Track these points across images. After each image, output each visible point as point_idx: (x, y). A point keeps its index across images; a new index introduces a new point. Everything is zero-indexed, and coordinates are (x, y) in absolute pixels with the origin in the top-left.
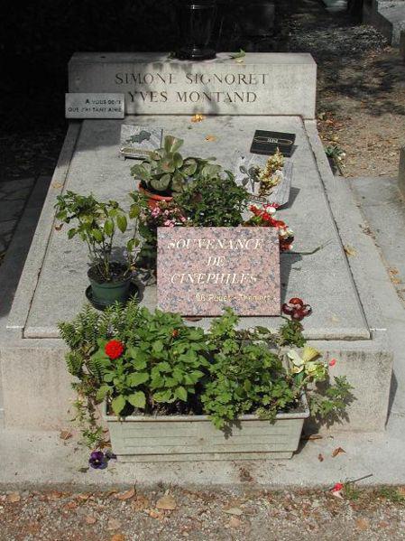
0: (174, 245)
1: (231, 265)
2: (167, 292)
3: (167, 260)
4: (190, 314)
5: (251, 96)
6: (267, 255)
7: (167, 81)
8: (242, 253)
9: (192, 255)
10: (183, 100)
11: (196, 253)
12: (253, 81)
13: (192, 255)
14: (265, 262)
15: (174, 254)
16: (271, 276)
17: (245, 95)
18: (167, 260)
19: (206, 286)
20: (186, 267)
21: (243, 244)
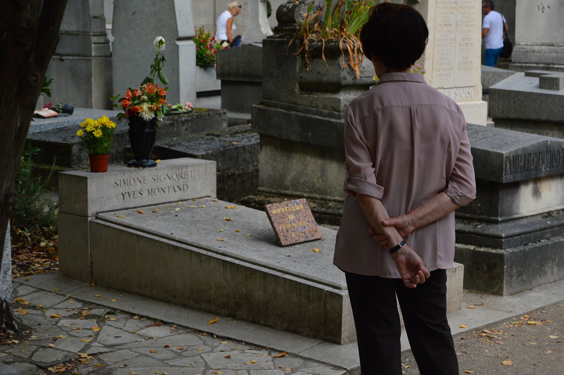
1: (298, 218)
10: (151, 193)
17: (182, 186)
18: (275, 220)
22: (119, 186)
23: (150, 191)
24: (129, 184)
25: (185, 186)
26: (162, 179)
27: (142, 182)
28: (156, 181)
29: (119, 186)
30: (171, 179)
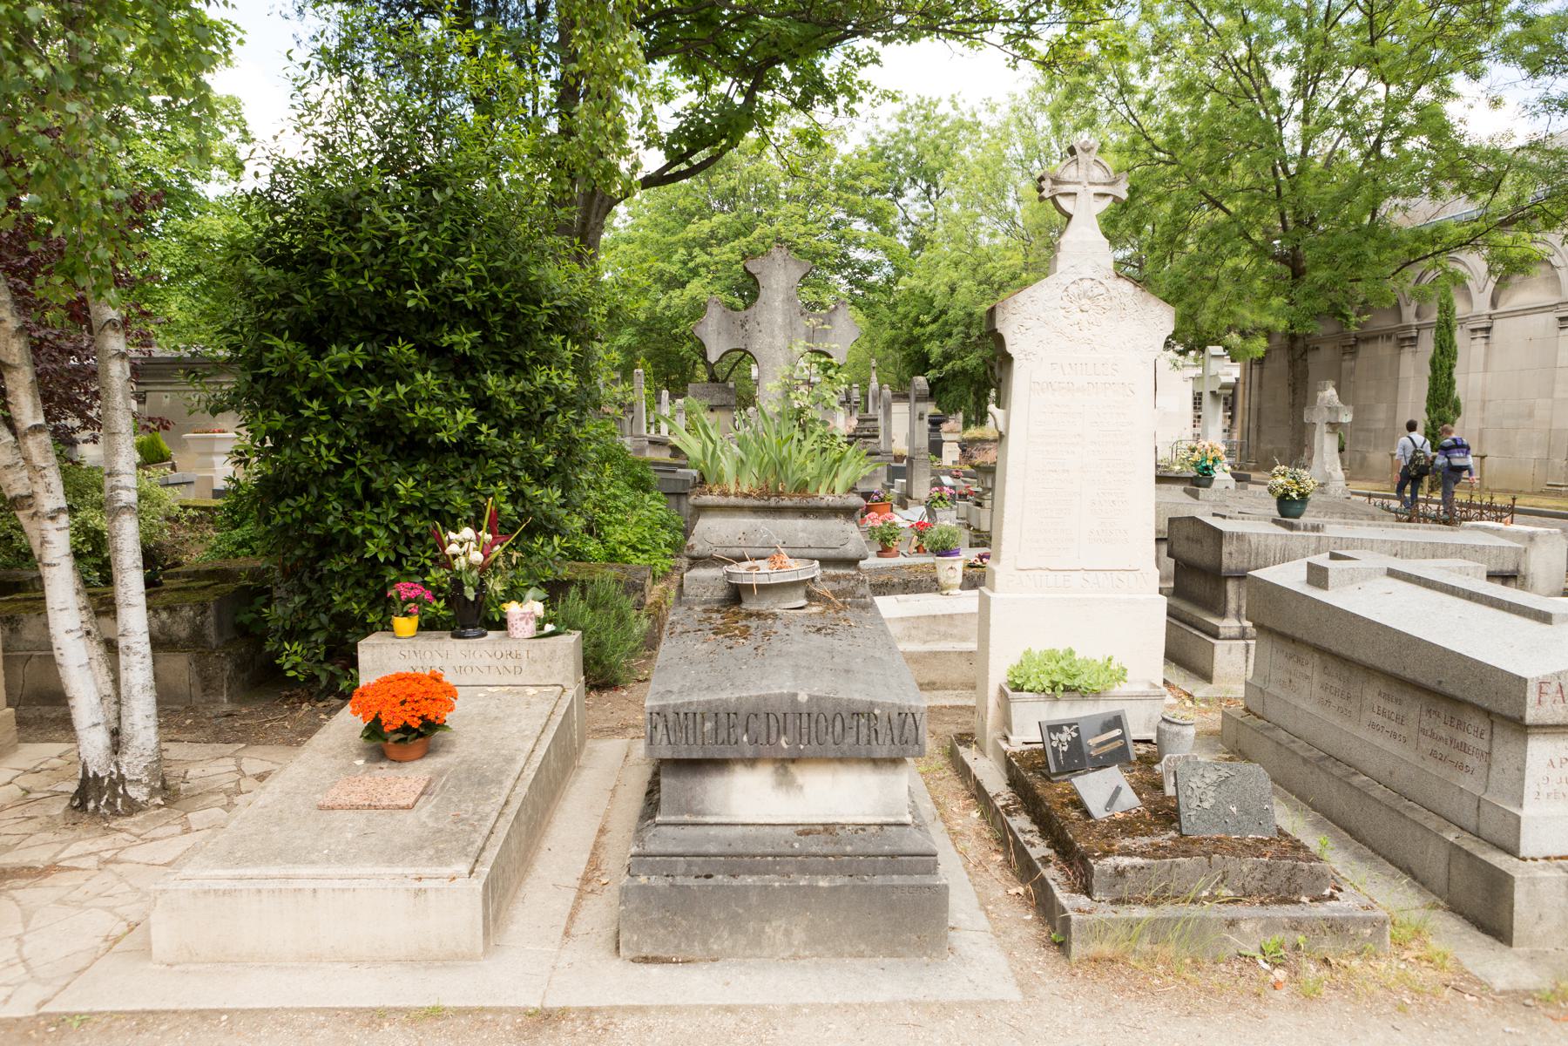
5: (518, 670)
25: (518, 670)
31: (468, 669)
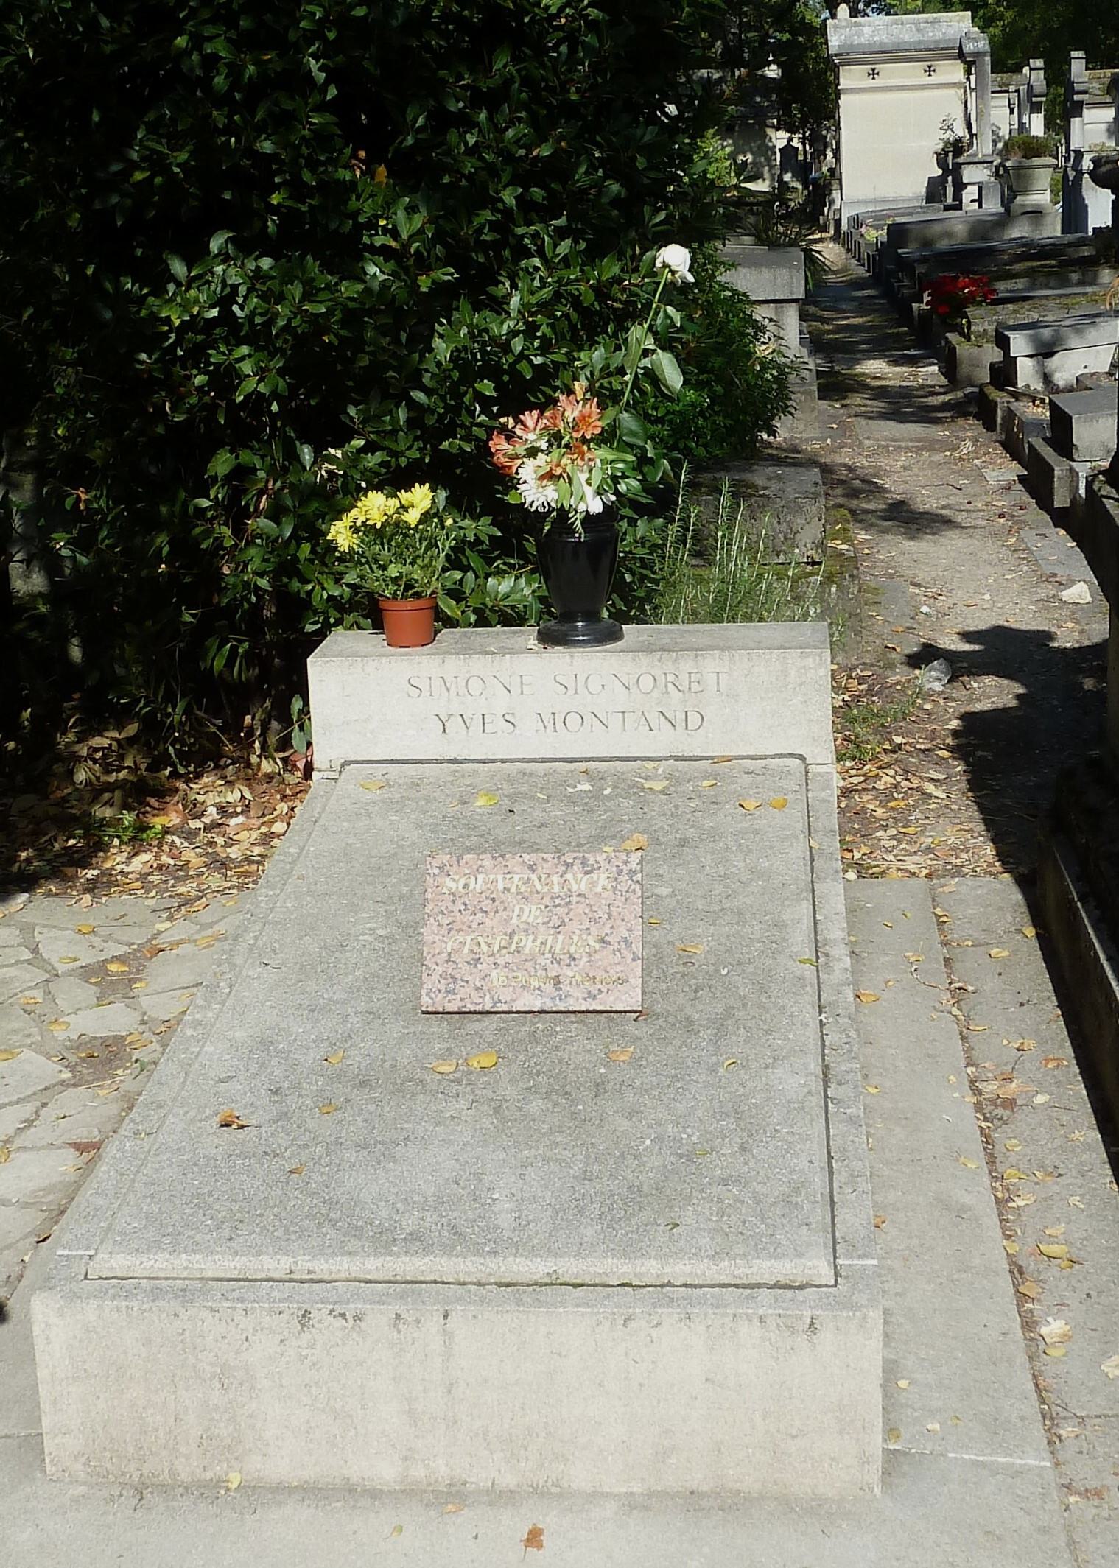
0: (453, 885)
1: (556, 921)
2: (440, 970)
3: (442, 912)
4: (478, 1008)
5: (694, 719)
6: (619, 901)
7: (515, 690)
8: (574, 899)
9: (487, 905)
11: (493, 900)
12: (695, 687)
13: (487, 905)
14: (614, 914)
15: (453, 902)
16: (626, 940)
18: (442, 912)
19: (509, 959)
20: (475, 925)
21: (578, 881)
22: (426, 693)
23: (547, 718)
24: (463, 691)
26: (594, 686)
27: (515, 690)
28: (571, 691)
29: (426, 693)
30: (634, 689)
31: (573, 720)
